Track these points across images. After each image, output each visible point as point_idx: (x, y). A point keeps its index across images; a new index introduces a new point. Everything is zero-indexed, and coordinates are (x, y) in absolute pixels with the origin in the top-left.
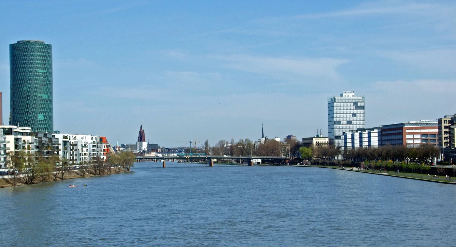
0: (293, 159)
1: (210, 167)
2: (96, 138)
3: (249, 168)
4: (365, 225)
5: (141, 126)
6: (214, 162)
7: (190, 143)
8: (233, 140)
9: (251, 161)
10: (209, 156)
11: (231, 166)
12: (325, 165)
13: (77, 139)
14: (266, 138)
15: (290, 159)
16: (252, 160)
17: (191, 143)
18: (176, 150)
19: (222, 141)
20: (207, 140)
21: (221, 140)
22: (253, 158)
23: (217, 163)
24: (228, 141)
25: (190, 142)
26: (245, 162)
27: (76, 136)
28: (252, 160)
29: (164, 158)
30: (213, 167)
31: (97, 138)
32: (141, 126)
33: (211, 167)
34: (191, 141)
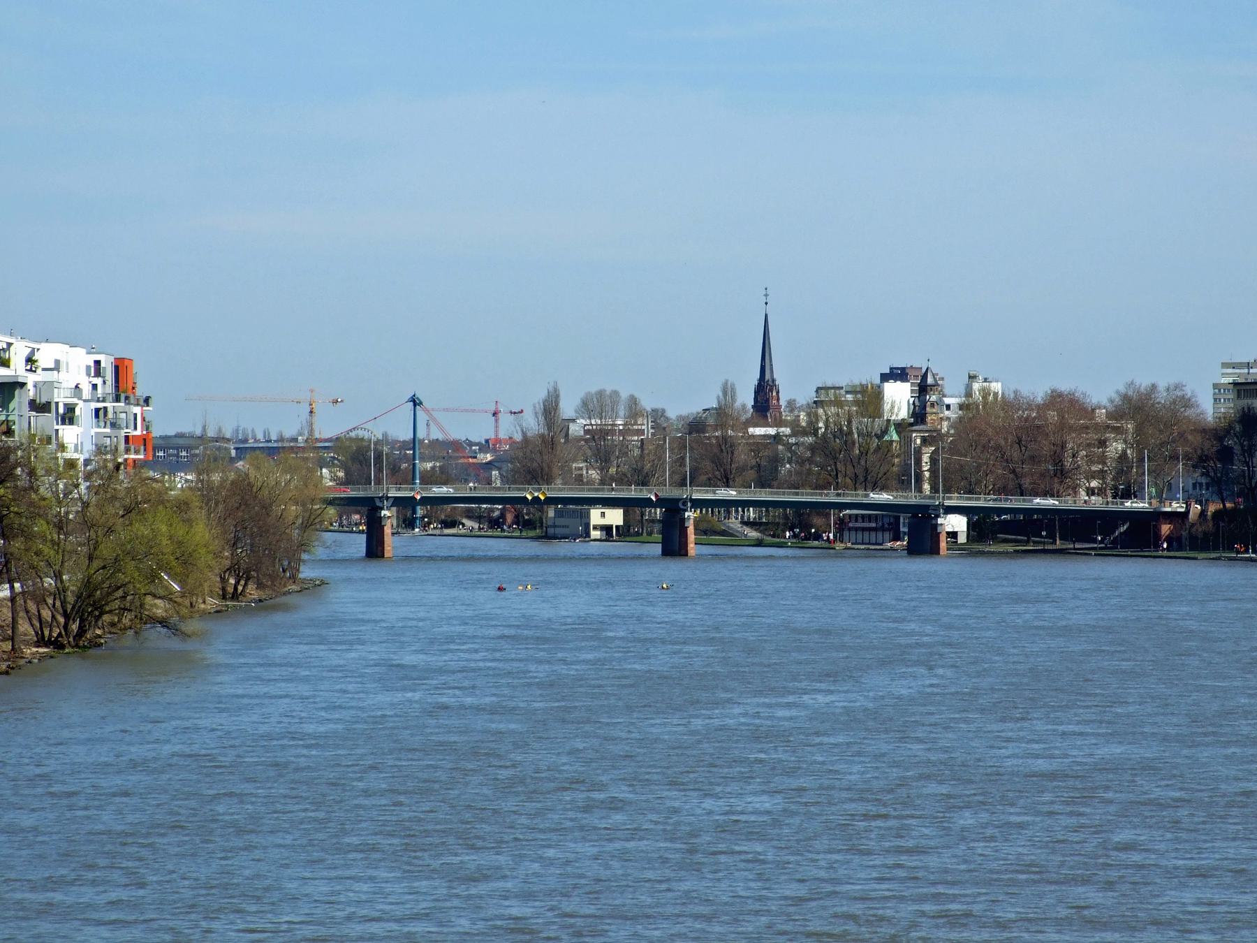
0: (1203, 513)
1: (375, 569)
2: (97, 363)
3: (921, 565)
4: (609, 924)
5: (766, 316)
6: (607, 529)
7: (415, 405)
8: (733, 390)
9: (936, 525)
10: (1142, 505)
11: (535, 559)
12: (1186, 550)
13: (39, 371)
14: (930, 380)
15: (1187, 513)
16: (940, 521)
17: (421, 403)
18: (179, 448)
19: (601, 393)
20: (556, 390)
21: (594, 389)
22: (947, 503)
23: (624, 532)
24: (637, 395)
25: (415, 402)
26: (856, 529)
27: (33, 352)
28: (940, 521)
29: (388, 498)
30: (692, 557)
31: (103, 365)
32: (766, 316)
33: (683, 559)
34: (421, 396)
